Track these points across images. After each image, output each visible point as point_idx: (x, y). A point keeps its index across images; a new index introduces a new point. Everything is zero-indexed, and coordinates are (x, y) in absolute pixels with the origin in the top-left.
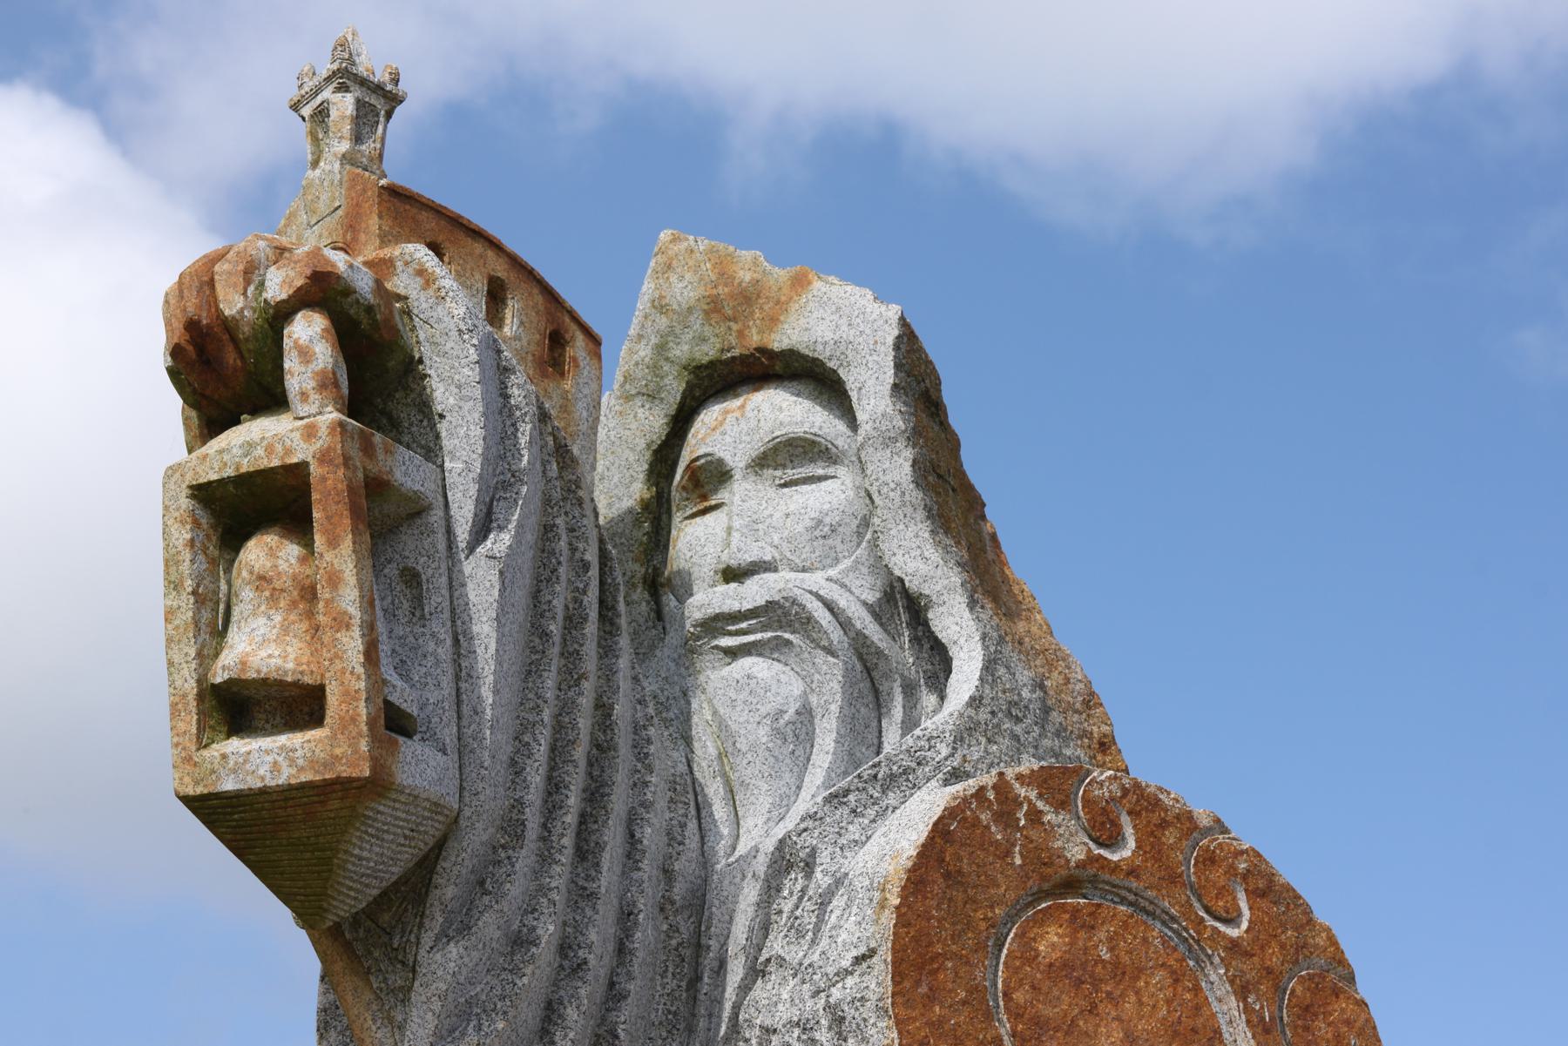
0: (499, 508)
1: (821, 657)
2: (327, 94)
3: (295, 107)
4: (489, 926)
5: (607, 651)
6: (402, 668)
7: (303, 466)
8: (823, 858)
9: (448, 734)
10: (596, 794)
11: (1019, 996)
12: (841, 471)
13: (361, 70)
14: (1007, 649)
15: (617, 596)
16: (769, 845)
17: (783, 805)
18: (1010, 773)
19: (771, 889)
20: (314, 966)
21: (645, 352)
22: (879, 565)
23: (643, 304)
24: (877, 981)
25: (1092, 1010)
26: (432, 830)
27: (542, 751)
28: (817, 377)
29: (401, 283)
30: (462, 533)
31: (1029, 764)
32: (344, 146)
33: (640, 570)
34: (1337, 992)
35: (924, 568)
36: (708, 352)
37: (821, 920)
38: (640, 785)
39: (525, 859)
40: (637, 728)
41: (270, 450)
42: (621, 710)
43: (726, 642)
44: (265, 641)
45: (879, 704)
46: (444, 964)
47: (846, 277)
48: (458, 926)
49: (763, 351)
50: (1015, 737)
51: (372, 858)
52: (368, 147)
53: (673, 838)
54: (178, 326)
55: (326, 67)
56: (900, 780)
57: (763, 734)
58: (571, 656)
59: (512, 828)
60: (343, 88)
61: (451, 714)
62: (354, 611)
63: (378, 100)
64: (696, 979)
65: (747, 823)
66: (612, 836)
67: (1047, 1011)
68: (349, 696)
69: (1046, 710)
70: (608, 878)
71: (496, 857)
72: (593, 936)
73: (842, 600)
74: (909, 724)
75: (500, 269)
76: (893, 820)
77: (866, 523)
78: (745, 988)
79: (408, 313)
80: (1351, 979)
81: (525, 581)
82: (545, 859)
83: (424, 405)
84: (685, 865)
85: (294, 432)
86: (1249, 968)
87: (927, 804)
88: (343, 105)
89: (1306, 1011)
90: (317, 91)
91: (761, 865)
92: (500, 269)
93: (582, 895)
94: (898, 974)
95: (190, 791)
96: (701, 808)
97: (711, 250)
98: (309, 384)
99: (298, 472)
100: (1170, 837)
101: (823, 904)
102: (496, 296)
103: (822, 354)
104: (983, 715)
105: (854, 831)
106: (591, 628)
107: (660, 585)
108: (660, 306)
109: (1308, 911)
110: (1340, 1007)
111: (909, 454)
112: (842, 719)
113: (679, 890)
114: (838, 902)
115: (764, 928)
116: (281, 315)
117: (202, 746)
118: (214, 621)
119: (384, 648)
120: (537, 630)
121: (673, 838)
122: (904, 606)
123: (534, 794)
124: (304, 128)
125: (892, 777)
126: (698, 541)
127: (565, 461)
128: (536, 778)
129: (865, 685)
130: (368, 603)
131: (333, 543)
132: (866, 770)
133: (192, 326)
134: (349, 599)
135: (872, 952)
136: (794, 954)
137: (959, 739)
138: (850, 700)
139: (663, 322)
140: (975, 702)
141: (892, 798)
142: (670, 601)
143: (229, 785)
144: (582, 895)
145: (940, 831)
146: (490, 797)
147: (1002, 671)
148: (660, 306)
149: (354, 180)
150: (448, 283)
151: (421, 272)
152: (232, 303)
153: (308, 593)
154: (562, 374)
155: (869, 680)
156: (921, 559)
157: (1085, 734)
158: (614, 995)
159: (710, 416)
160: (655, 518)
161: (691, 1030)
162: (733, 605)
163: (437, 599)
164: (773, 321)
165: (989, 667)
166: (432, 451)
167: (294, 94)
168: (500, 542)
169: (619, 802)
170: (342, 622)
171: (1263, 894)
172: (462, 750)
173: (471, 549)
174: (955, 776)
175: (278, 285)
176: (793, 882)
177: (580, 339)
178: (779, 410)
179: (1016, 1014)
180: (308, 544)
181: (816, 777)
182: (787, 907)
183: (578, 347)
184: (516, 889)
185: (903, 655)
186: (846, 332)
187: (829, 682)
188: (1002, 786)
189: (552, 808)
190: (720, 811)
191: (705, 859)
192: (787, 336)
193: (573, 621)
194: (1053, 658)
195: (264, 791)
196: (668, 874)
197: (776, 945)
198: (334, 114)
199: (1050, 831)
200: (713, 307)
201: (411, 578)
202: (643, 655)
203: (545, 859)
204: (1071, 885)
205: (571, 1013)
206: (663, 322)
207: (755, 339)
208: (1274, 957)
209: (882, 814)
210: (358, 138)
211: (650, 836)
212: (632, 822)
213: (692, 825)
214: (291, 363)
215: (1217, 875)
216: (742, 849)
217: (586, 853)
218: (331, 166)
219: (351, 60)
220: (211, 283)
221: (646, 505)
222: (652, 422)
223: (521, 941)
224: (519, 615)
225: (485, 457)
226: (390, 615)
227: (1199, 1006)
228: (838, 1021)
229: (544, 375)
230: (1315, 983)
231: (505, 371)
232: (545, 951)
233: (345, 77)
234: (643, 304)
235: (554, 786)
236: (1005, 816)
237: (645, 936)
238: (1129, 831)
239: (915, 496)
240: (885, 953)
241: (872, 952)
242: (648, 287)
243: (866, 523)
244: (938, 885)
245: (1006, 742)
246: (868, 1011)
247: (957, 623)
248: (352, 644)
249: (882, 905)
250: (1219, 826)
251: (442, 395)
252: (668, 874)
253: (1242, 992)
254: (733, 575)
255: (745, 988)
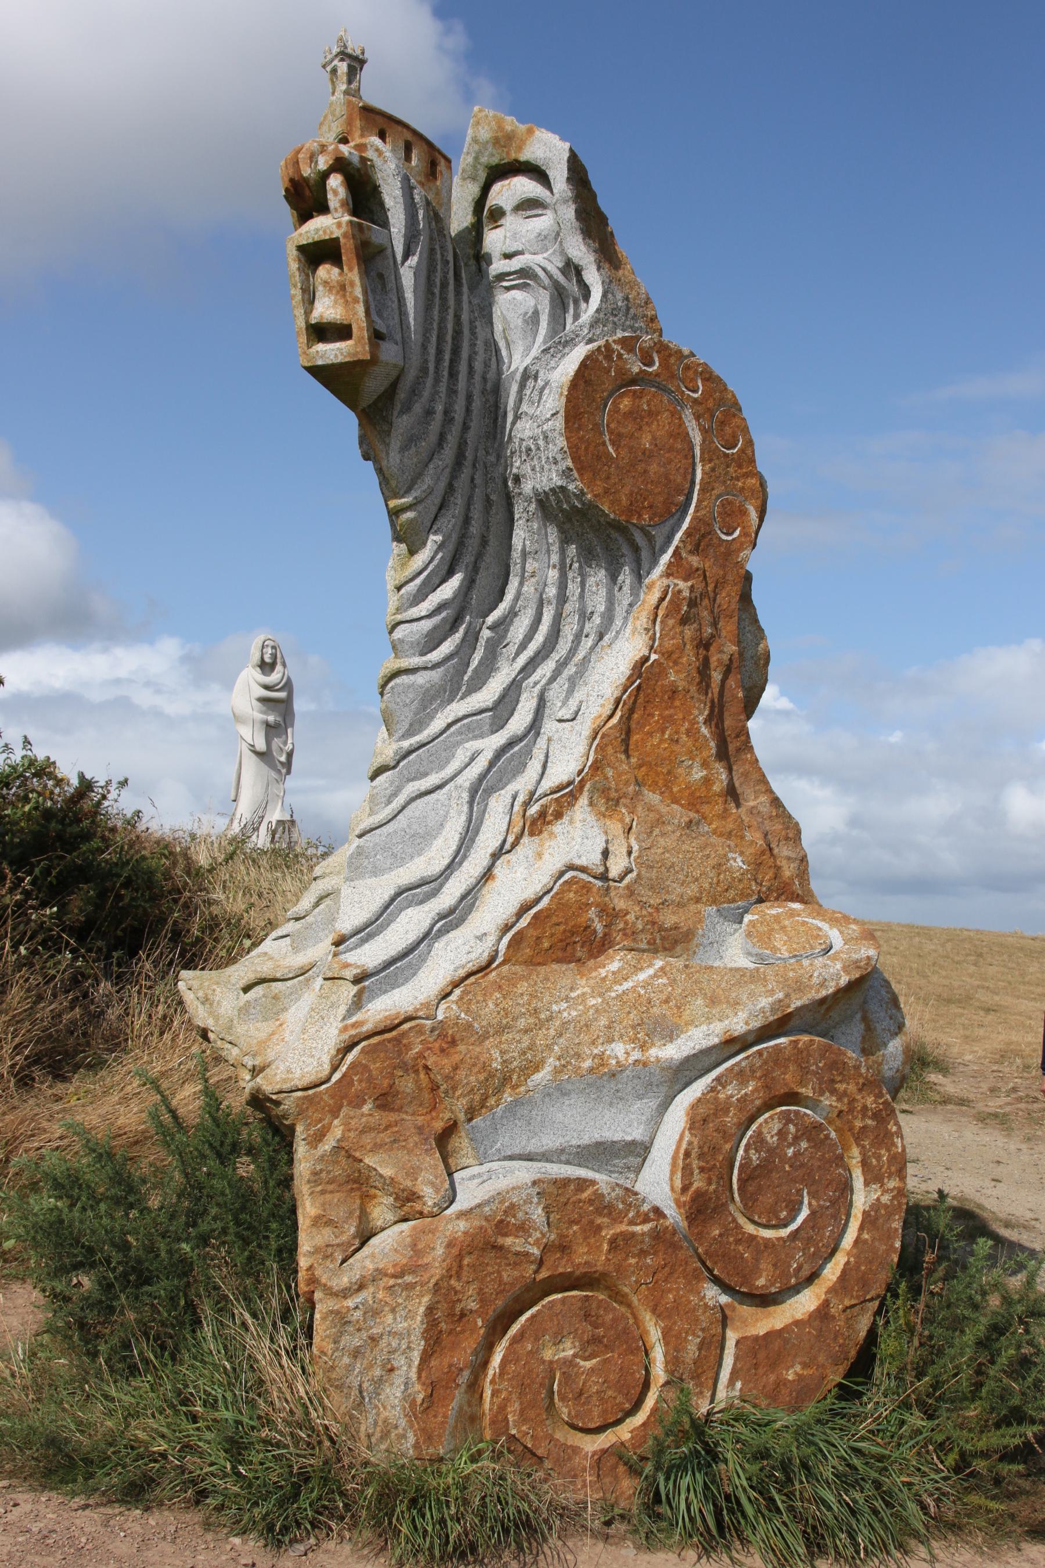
0: (412, 246)
1: (541, 290)
2: (336, 62)
3: (324, 67)
4: (418, 408)
5: (458, 293)
6: (379, 314)
7: (337, 239)
8: (541, 374)
9: (398, 337)
10: (456, 351)
11: (612, 426)
12: (548, 212)
13: (349, 51)
14: (613, 285)
15: (462, 267)
16: (521, 370)
17: (528, 349)
18: (611, 340)
19: (522, 386)
20: (356, 421)
21: (470, 159)
22: (563, 252)
23: (468, 139)
24: (559, 423)
25: (640, 428)
26: (395, 373)
27: (434, 339)
28: (537, 173)
29: (370, 154)
30: (399, 258)
31: (620, 334)
32: (344, 87)
33: (471, 252)
34: (734, 415)
35: (580, 254)
36: (495, 161)
37: (540, 398)
38: (473, 345)
39: (429, 381)
40: (471, 322)
41: (325, 232)
42: (465, 317)
43: (505, 284)
44: (328, 307)
45: (565, 309)
46: (403, 423)
47: (548, 129)
48: (407, 409)
49: (516, 161)
50: (614, 323)
51: (373, 386)
52: (354, 86)
53: (487, 365)
54: (287, 179)
55: (335, 50)
56: (569, 343)
57: (520, 322)
58: (444, 299)
59: (424, 370)
60: (342, 60)
61: (399, 329)
62: (360, 296)
63: (356, 63)
64: (496, 420)
65: (514, 357)
66: (463, 368)
67: (623, 430)
68: (360, 329)
69: (628, 309)
70: (462, 384)
71: (419, 382)
72: (457, 407)
73: (550, 267)
74: (577, 317)
75: (409, 136)
76: (567, 359)
77: (558, 234)
78: (514, 423)
79: (373, 166)
80: (740, 410)
81: (424, 273)
82: (437, 380)
83: (382, 204)
84: (491, 375)
85: (330, 224)
86: (701, 409)
87: (578, 353)
88: (343, 67)
89: (722, 423)
90: (332, 60)
91: (518, 377)
92: (409, 136)
93: (452, 392)
94: (567, 421)
95: (307, 364)
96: (497, 351)
97: (494, 117)
98: (338, 205)
99: (336, 241)
100: (672, 360)
101: (541, 393)
102: (408, 148)
103: (540, 163)
104: (602, 316)
105: (553, 364)
106: (451, 287)
107: (481, 259)
108: (475, 140)
109: (725, 385)
110: (735, 421)
111: (573, 207)
112: (550, 315)
113: (489, 386)
114: (546, 391)
115: (520, 400)
116: (325, 176)
117: (309, 347)
118: (310, 299)
119: (372, 307)
120: (429, 291)
121: (487, 365)
122: (572, 269)
123: (432, 358)
124: (327, 76)
125: (567, 342)
126: (494, 240)
127: (437, 219)
128: (432, 351)
129: (558, 301)
130: (365, 292)
131: (351, 270)
132: (556, 339)
133: (292, 180)
134: (358, 292)
135: (557, 413)
136: (531, 411)
137: (592, 326)
138: (553, 307)
139: (476, 147)
140: (598, 311)
141: (567, 350)
142: (484, 265)
143: (320, 362)
144: (452, 392)
145: (583, 365)
146: (415, 361)
147: (610, 296)
148: (475, 140)
149: (349, 103)
150: (388, 154)
151: (377, 150)
152: (306, 172)
153: (343, 287)
154: (436, 178)
155: (561, 301)
156: (580, 251)
157: (645, 316)
158: (466, 427)
159: (496, 187)
160: (476, 232)
161: (495, 438)
162: (507, 269)
163: (391, 284)
164: (520, 149)
165: (605, 295)
166: (385, 224)
167: (324, 61)
168: (413, 261)
169: (465, 354)
170: (356, 300)
171: (708, 380)
172: (404, 342)
173: (403, 263)
174: (590, 341)
175: (323, 163)
176: (530, 383)
177: (443, 162)
178: (522, 186)
179: (611, 433)
180: (341, 268)
181: (540, 338)
182: (528, 392)
183: (442, 166)
184: (426, 394)
185: (574, 288)
186: (549, 154)
187: (543, 301)
188: (607, 345)
189: (439, 360)
190: (504, 353)
191: (499, 373)
192: (525, 156)
193: (444, 285)
194: (633, 285)
195: (333, 365)
196: (484, 379)
197: (524, 407)
198: (339, 72)
199: (626, 361)
200: (496, 141)
201: (381, 276)
202: (472, 289)
203: (437, 380)
204: (634, 381)
205: (449, 437)
206: (476, 147)
207: (513, 156)
208: (710, 404)
209: (563, 356)
210: (350, 82)
211: (478, 365)
212: (471, 360)
213: (494, 359)
214: (330, 196)
215: (690, 374)
216: (512, 369)
217: (453, 375)
218: (339, 95)
219: (346, 47)
220: (297, 162)
221: (473, 225)
222: (473, 190)
223: (429, 412)
224: (422, 287)
225: (406, 227)
226: (374, 291)
227: (681, 424)
228: (546, 437)
229: (428, 180)
230: (726, 413)
231: (412, 188)
232: (439, 416)
233: (343, 55)
234: (468, 139)
235: (439, 352)
236: (608, 357)
237: (477, 404)
238: (656, 359)
239: (576, 224)
240: (562, 413)
241: (557, 413)
242: (470, 131)
243: (558, 234)
244: (581, 382)
245: (610, 326)
246: (556, 434)
247: (593, 278)
248: (360, 309)
249: (561, 394)
250: (692, 355)
251: (389, 202)
252: (484, 379)
253: (697, 417)
254: (508, 256)
255: (514, 423)
